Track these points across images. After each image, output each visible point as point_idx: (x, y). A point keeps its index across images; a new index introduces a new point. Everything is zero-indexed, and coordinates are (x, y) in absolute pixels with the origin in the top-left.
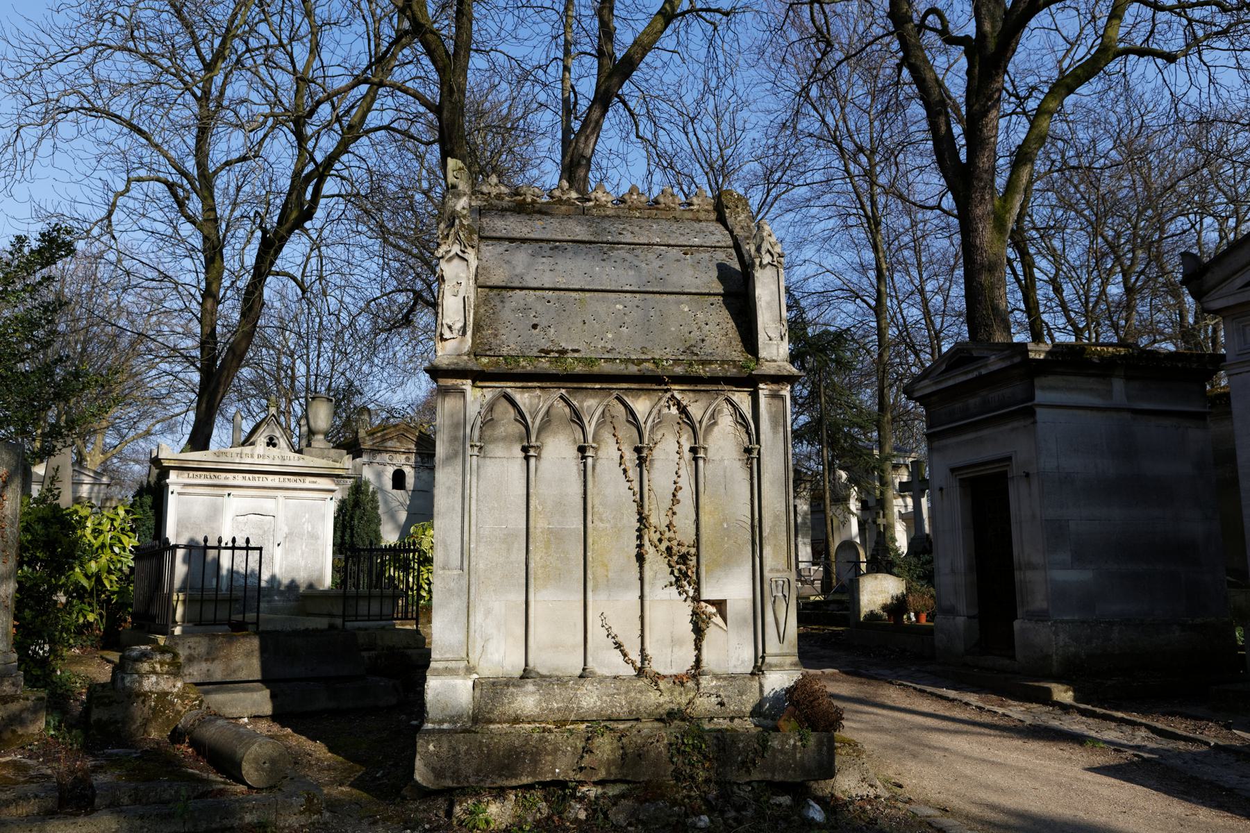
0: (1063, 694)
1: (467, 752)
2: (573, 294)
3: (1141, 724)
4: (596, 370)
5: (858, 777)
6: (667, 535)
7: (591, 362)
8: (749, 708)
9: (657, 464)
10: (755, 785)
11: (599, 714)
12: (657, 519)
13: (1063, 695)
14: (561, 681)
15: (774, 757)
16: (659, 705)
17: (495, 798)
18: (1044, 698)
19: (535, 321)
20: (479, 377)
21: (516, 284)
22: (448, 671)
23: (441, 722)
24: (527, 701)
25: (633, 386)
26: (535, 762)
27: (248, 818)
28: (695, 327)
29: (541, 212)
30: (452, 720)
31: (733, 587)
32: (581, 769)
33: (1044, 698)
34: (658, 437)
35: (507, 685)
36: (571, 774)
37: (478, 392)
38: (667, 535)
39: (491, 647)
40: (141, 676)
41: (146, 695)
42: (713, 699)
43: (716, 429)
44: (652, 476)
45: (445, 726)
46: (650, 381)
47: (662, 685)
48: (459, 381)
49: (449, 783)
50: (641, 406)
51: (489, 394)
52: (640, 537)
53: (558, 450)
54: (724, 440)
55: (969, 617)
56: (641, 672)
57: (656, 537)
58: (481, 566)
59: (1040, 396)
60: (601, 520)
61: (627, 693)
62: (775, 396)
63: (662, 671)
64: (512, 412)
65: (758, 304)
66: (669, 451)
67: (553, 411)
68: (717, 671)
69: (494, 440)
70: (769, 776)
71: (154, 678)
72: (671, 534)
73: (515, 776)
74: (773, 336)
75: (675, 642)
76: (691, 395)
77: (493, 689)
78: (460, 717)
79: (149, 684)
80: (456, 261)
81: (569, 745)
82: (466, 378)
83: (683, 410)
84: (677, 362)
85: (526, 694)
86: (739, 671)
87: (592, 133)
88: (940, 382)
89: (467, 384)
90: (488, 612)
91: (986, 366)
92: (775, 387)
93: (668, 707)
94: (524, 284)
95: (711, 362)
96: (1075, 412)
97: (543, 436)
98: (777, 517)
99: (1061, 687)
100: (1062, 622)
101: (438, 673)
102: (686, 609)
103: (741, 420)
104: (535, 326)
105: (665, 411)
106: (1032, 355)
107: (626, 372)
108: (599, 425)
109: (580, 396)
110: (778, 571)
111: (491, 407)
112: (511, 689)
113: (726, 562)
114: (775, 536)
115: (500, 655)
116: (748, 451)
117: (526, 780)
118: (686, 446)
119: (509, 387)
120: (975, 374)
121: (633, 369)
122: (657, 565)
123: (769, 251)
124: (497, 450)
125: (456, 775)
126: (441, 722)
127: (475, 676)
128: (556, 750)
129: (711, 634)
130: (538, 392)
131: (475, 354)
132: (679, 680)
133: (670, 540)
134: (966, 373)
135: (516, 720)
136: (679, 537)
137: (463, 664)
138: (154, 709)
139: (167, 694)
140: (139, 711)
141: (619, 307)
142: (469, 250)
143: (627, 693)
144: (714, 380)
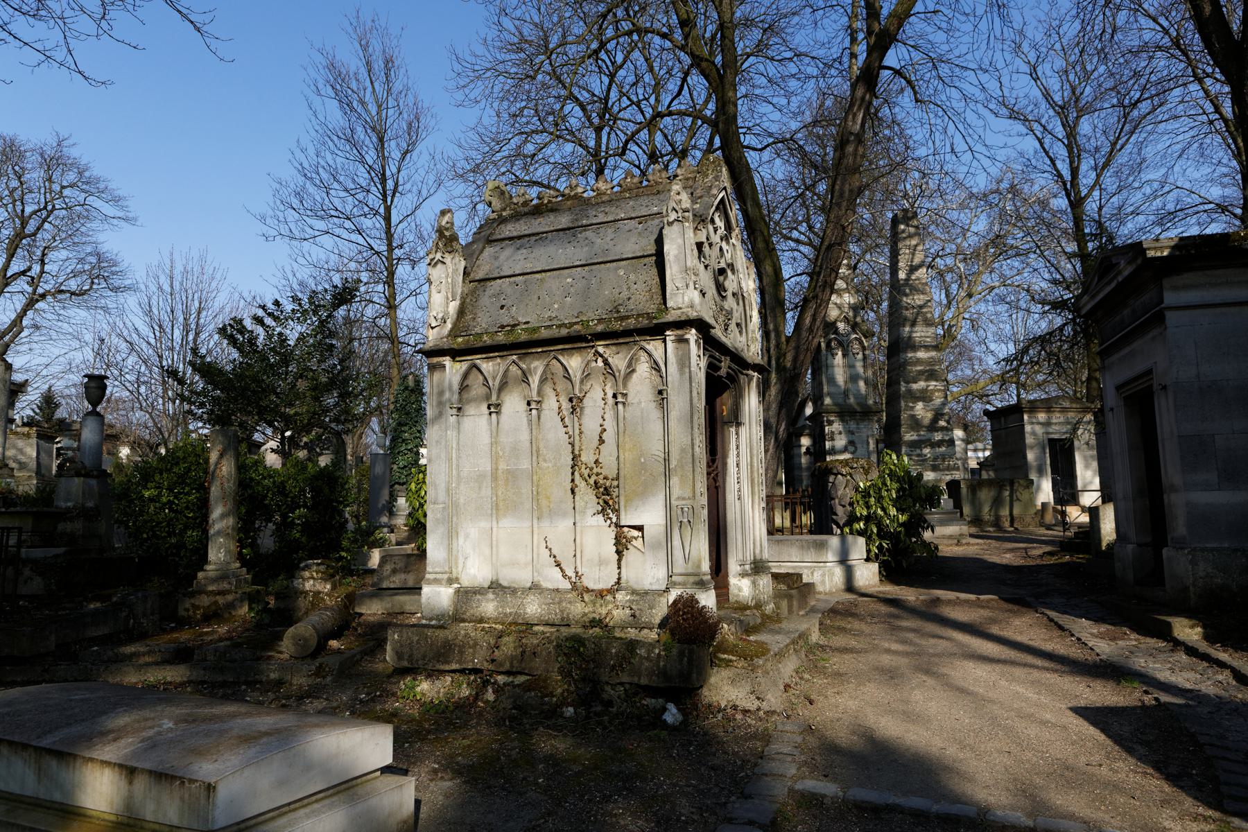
0: (1188, 631)
1: (418, 642)
2: (538, 276)
3: (1222, 665)
4: (536, 336)
5: (748, 689)
6: (595, 470)
7: (535, 330)
8: (657, 621)
9: (587, 411)
10: (627, 686)
11: (539, 619)
12: (587, 457)
13: (1188, 631)
14: (513, 591)
15: (642, 664)
16: (585, 614)
17: (427, 678)
18: (1164, 633)
19: (504, 303)
20: (455, 354)
21: (497, 275)
22: (437, 581)
23: (431, 619)
24: (489, 607)
25: (567, 346)
26: (461, 653)
27: (272, 676)
28: (625, 287)
29: (552, 210)
30: (438, 618)
31: (649, 514)
32: (493, 661)
33: (1164, 633)
34: (586, 388)
35: (475, 593)
36: (486, 664)
37: (458, 365)
38: (595, 470)
39: (469, 563)
40: (304, 580)
41: (306, 593)
42: (628, 611)
43: (635, 376)
44: (583, 421)
45: (433, 622)
46: (576, 340)
47: (586, 597)
48: (441, 359)
49: (405, 664)
50: (574, 363)
51: (465, 366)
52: (573, 474)
53: (513, 404)
54: (641, 384)
55: (1139, 545)
56: (574, 587)
57: (586, 472)
58: (462, 501)
59: (1170, 298)
60: (545, 461)
61: (559, 603)
62: (682, 340)
63: (591, 586)
64: (481, 378)
65: (666, 258)
66: (596, 396)
67: (510, 374)
68: (636, 587)
69: (469, 401)
70: (636, 680)
71: (311, 582)
72: (599, 470)
73: (448, 663)
74: (680, 285)
75: (602, 562)
76: (614, 348)
77: (466, 595)
78: (443, 616)
79: (308, 585)
80: (439, 265)
81: (485, 641)
82: (445, 355)
83: (606, 362)
84: (600, 321)
85: (488, 600)
86: (654, 588)
87: (859, 109)
88: (1098, 292)
89: (447, 361)
90: (467, 536)
91: (1120, 273)
92: (679, 332)
93: (591, 616)
94: (502, 274)
95: (628, 317)
96: (1224, 310)
97: (502, 394)
98: (683, 450)
99: (1185, 621)
100: (1203, 550)
101: (430, 582)
102: (611, 534)
103: (656, 367)
104: (502, 307)
105: (594, 364)
106: (1151, 254)
107: (557, 335)
108: (543, 381)
109: (528, 360)
110: (684, 499)
111: (466, 376)
112: (478, 597)
113: (643, 493)
114: (682, 467)
115: (475, 571)
116: (660, 392)
117: (454, 666)
118: (610, 394)
119: (478, 359)
120: (1113, 285)
121: (564, 332)
122: (587, 497)
123: (674, 209)
124: (470, 410)
125: (410, 659)
126: (431, 619)
127: (456, 586)
128: (476, 644)
129: (629, 556)
130: (499, 360)
131: (454, 334)
132: (601, 594)
133: (598, 474)
134: (1109, 283)
135: (481, 621)
136: (604, 472)
137: (446, 576)
138: (312, 603)
139: (319, 592)
140: (302, 603)
141: (569, 280)
142: (447, 255)
143: (559, 603)
144: (627, 333)
